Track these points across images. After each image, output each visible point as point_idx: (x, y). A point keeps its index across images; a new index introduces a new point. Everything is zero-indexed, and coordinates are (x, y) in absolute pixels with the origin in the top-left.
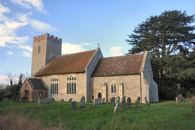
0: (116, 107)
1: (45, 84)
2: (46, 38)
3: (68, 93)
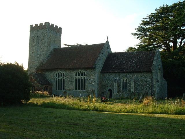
0: (95, 103)
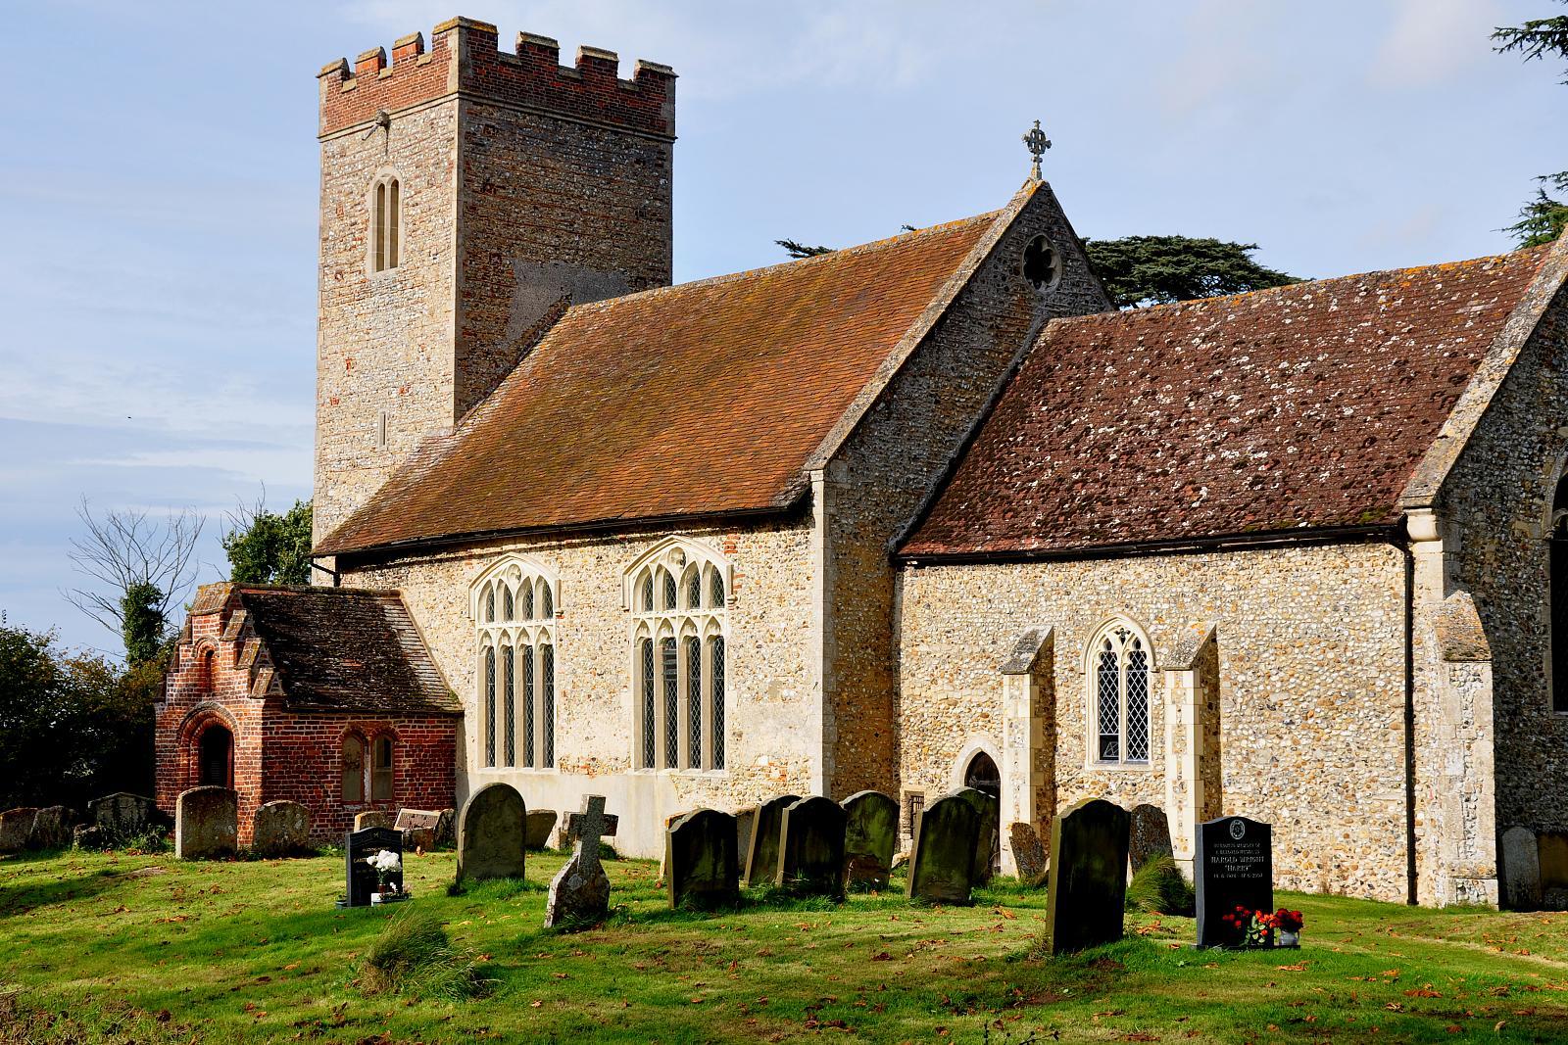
1: (424, 652)
2: (453, 84)
3: (650, 762)
